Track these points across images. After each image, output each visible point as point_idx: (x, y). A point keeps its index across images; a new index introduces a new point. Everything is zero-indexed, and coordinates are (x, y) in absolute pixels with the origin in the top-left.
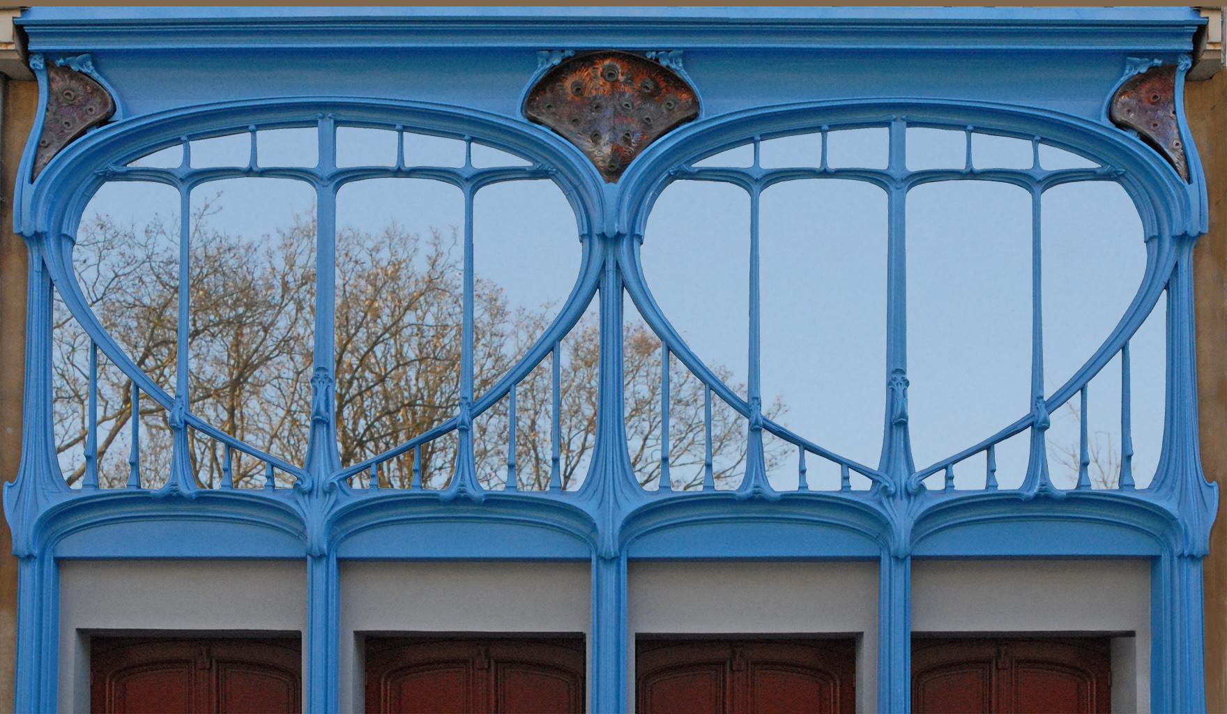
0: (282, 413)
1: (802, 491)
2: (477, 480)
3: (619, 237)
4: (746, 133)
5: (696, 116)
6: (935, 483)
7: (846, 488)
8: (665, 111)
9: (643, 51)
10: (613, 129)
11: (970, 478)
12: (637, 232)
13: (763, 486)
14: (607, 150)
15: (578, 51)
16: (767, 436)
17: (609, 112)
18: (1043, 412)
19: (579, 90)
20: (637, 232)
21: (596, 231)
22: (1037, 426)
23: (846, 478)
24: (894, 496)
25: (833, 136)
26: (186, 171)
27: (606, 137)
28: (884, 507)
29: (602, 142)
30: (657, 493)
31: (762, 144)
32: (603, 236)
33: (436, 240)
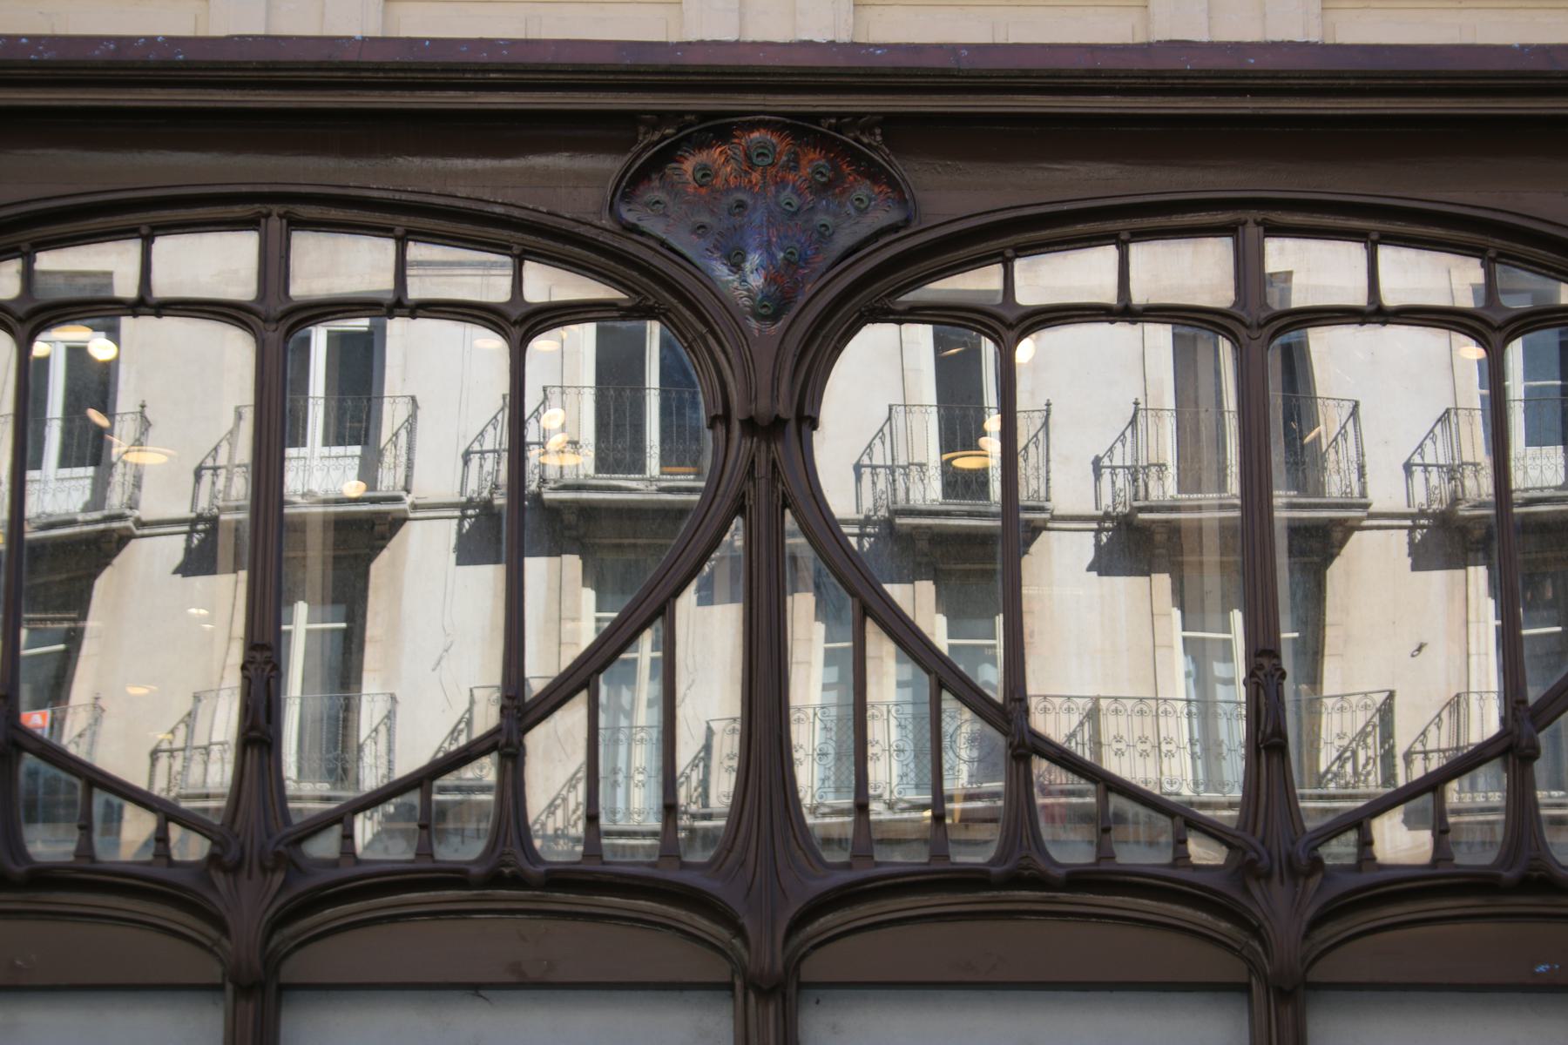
0: (1335, 754)
1: (1104, 867)
2: (1505, 257)
3: (778, 424)
4: (994, 245)
5: (907, 222)
6: (1341, 850)
7: (1181, 856)
8: (852, 211)
9: (815, 117)
10: (767, 247)
11: (1400, 841)
12: (806, 413)
13: (1036, 856)
14: (756, 281)
15: (705, 116)
16: (1040, 767)
17: (758, 217)
18: (1528, 726)
19: (705, 172)
20: (806, 413)
21: (737, 415)
22: (506, 743)
23: (1181, 842)
24: (1268, 876)
25: (1137, 252)
26: (29, 306)
27: (754, 259)
28: (1251, 897)
29: (748, 266)
30: (847, 866)
31: (1019, 265)
32: (750, 425)
33: (710, 733)
